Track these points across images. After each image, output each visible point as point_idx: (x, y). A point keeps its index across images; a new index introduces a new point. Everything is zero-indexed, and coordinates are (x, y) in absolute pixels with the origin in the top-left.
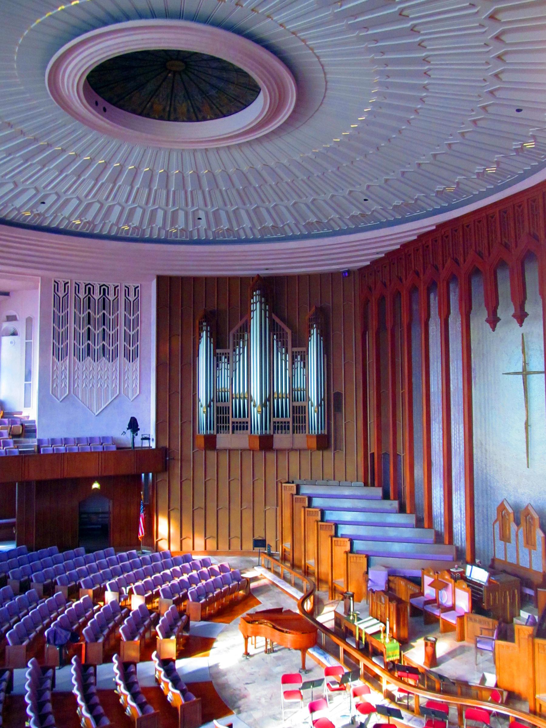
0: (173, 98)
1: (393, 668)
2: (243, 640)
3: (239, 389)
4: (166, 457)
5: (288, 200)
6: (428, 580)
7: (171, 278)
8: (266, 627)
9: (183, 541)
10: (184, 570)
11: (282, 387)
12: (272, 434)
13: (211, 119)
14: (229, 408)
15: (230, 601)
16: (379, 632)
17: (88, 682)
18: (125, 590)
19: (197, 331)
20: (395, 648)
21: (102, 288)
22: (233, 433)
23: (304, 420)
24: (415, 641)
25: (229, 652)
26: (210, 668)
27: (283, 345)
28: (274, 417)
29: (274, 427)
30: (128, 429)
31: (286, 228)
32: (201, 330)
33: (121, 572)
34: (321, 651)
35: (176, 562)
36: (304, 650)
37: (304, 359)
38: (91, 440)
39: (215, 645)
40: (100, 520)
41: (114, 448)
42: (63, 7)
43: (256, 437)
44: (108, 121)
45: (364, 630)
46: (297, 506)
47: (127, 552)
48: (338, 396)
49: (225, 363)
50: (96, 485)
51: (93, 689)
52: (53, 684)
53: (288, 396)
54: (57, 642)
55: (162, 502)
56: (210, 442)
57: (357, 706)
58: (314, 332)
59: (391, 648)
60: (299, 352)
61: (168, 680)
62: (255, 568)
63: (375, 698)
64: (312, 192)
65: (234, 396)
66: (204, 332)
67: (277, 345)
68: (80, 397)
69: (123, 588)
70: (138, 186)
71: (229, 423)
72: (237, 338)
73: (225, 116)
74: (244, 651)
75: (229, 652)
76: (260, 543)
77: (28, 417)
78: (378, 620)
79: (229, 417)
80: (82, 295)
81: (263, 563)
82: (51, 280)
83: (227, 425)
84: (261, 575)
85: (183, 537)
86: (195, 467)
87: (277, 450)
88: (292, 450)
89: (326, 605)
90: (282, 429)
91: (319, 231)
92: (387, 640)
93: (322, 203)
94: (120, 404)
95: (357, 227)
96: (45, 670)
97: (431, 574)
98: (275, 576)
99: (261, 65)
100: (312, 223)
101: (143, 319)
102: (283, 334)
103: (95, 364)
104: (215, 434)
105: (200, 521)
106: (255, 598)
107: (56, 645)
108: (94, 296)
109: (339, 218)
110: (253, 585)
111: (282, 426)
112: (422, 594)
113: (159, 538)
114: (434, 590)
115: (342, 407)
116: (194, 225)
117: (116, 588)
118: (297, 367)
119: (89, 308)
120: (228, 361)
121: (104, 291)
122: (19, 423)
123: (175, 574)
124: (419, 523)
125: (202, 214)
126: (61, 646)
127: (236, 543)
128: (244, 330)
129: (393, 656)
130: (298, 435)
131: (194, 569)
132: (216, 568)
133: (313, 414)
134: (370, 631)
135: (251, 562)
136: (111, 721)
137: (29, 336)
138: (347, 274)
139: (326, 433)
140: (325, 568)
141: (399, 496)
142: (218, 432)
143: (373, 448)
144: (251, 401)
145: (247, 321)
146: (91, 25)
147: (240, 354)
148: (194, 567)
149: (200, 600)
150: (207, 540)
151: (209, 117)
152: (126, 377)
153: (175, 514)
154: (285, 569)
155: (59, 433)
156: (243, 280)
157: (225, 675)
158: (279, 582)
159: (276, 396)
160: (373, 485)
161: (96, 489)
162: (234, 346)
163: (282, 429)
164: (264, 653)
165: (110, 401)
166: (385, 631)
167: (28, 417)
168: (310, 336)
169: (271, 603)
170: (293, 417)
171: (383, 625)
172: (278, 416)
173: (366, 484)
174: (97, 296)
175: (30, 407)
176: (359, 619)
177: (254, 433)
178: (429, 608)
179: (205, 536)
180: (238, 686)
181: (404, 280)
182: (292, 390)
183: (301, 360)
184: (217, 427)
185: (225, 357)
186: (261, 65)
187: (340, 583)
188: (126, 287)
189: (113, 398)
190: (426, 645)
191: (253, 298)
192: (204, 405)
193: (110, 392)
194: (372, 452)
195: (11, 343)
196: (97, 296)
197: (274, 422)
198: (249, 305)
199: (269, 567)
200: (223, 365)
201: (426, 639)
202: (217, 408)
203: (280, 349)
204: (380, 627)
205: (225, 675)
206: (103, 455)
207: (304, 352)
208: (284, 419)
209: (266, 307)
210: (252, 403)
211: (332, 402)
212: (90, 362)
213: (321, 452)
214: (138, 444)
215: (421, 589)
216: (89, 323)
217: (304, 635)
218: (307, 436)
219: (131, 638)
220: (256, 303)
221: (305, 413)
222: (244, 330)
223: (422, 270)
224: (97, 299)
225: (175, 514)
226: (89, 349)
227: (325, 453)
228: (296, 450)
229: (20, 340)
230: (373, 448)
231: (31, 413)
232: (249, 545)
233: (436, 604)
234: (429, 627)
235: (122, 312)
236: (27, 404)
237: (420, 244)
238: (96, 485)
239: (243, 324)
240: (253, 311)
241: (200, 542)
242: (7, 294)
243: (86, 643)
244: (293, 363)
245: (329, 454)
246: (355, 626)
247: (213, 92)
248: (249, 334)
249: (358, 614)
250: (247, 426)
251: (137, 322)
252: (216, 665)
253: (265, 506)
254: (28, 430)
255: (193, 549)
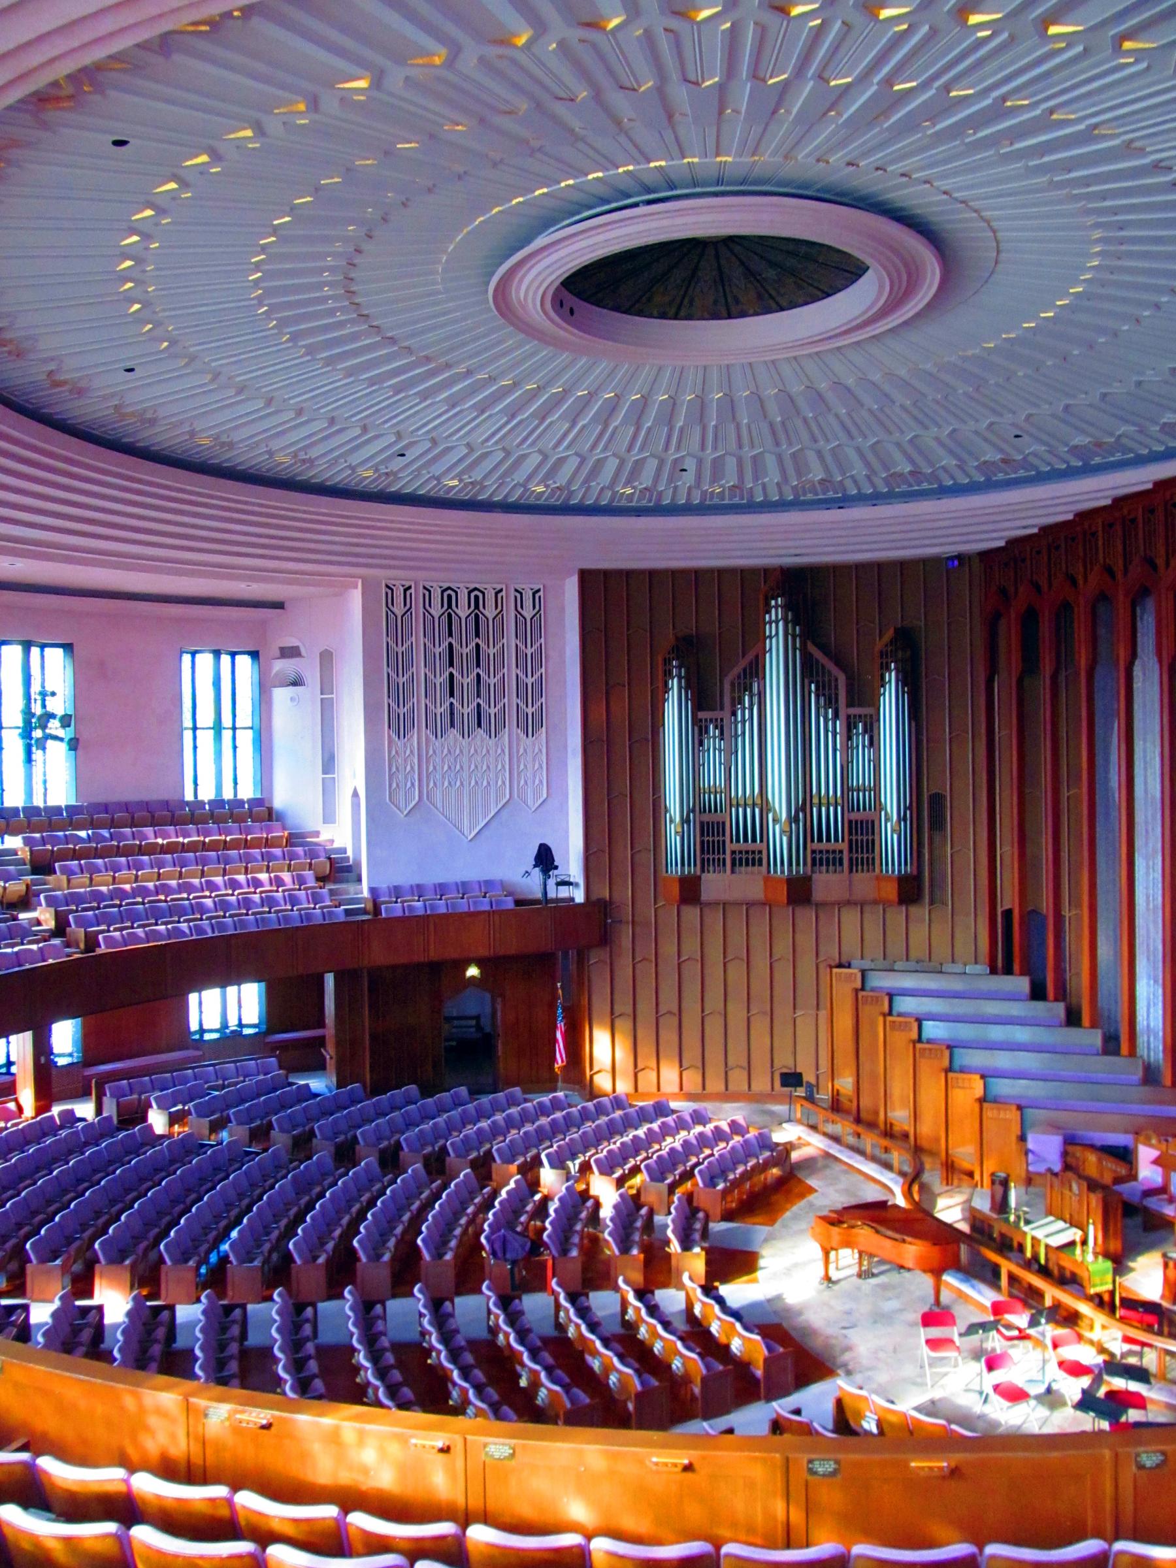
0: (693, 284)
1: (1105, 1303)
2: (819, 1254)
3: (745, 785)
4: (606, 918)
5: (865, 437)
6: (1146, 1154)
7: (606, 574)
8: (864, 1234)
9: (640, 1075)
10: (666, 1131)
11: (826, 778)
12: (809, 873)
13: (756, 314)
14: (724, 823)
15: (768, 1188)
16: (1072, 1244)
17: (374, 1331)
18: (574, 1166)
19: (660, 673)
20: (1105, 1272)
21: (472, 595)
22: (733, 872)
23: (870, 846)
24: (1134, 1260)
25: (793, 1271)
26: (769, 1301)
27: (830, 702)
28: (812, 840)
29: (814, 860)
30: (535, 866)
31: (849, 484)
32: (668, 674)
33: (461, 1125)
34: (960, 1275)
35: (643, 1116)
36: (937, 1272)
37: (872, 730)
38: (464, 888)
39: (762, 1262)
40: (454, 1030)
41: (509, 904)
42: (571, 182)
43: (779, 880)
44: (576, 331)
45: (1044, 1241)
46: (866, 1011)
47: (551, 1096)
48: (937, 801)
49: (714, 737)
50: (473, 971)
51: (385, 1342)
52: (244, 1335)
53: (839, 801)
54: (508, 1256)
55: (600, 1004)
56: (689, 891)
57: (1061, 1364)
58: (892, 677)
59: (1098, 1272)
60: (860, 716)
61: (509, 1330)
62: (784, 1125)
63: (1088, 1356)
64: (912, 423)
65: (734, 802)
66: (675, 680)
67: (817, 702)
68: (439, 805)
69: (570, 1164)
70: (585, 422)
71: (724, 853)
72: (739, 691)
73: (782, 309)
74: (822, 1273)
75: (793, 1271)
76: (792, 1079)
77: (332, 841)
78: (1065, 1221)
79: (724, 842)
80: (436, 610)
81: (799, 1115)
82: (379, 583)
83: (721, 857)
84: (800, 1138)
85: (640, 1066)
86: (660, 938)
87: (817, 905)
88: (849, 903)
89: (939, 1195)
90: (828, 865)
91: (911, 486)
92: (1090, 1257)
93: (934, 444)
94: (518, 818)
95: (988, 480)
96: (299, 1308)
97: (1154, 1141)
98: (830, 1142)
99: (892, 249)
100: (901, 475)
101: (551, 653)
102: (830, 681)
103: (465, 742)
104: (698, 873)
105: (669, 1036)
106: (800, 1181)
107: (506, 1260)
108: (458, 612)
109: (959, 466)
110: (795, 1156)
111: (828, 859)
112: (1132, 1176)
113: (596, 1069)
114: (1159, 1169)
115: (946, 823)
116: (671, 480)
117: (558, 1163)
118: (858, 746)
119: (450, 635)
120: (722, 733)
121: (476, 600)
122: (323, 854)
123: (652, 1137)
124: (1111, 1045)
125: (690, 464)
126: (514, 1263)
127: (738, 1080)
128: (751, 673)
129: (1102, 1284)
130: (860, 875)
131: (683, 1129)
132: (724, 1126)
133: (891, 835)
134: (1056, 1241)
135: (771, 1114)
136: (660, 1381)
137: (327, 686)
138: (956, 562)
139: (915, 873)
140: (928, 1128)
141: (1062, 993)
142: (703, 871)
143: (1008, 899)
144: (768, 810)
145: (757, 656)
146: (601, 199)
147: (743, 722)
148: (682, 1125)
149: (666, 1179)
150: (684, 1073)
151: (751, 311)
152: (522, 767)
153: (623, 1025)
154: (841, 1127)
155: (404, 875)
156: (745, 575)
157: (800, 1313)
158: (840, 1151)
159: (816, 800)
160: (1008, 971)
161: (473, 977)
162: (733, 705)
163: (828, 865)
164: (855, 1279)
165: (493, 813)
166: (1084, 1242)
167: (332, 841)
168: (883, 686)
169: (836, 1191)
170: (850, 841)
171: (1080, 1233)
172: (820, 839)
173: (993, 971)
174: (463, 611)
175: (334, 822)
176: (1027, 1222)
177: (775, 871)
178: (1152, 1203)
179: (681, 1066)
180: (831, 1331)
181: (1081, 582)
182: (847, 789)
183: (865, 731)
184: (703, 860)
185: (716, 727)
186: (892, 249)
187: (965, 1153)
188: (516, 590)
189: (500, 806)
190: (1166, 1266)
191: (769, 612)
192: (678, 819)
193: (493, 796)
194: (1007, 907)
195: (292, 699)
196: (463, 611)
197: (813, 852)
198: (761, 625)
199: (811, 1122)
200: (712, 742)
201: (1164, 1256)
202: (702, 824)
203: (822, 711)
204: (1075, 1234)
205: (800, 1313)
206: (497, 918)
207: (871, 716)
208: (832, 845)
209: (794, 630)
210: (770, 816)
211: (927, 811)
212: (456, 740)
213: (904, 908)
214: (552, 894)
215: (1131, 1169)
216: (451, 664)
217: (937, 1247)
218: (878, 878)
219: (625, 1249)
220: (777, 622)
221: (873, 833)
222: (751, 673)
223: (1121, 562)
224: (463, 615)
225: (623, 1025)
226: (452, 714)
227: (914, 910)
228: (856, 904)
229: (310, 692)
230: (1008, 899)
231: (341, 834)
232: (761, 1084)
233: (1165, 1196)
234: (1153, 1236)
235: (510, 640)
236: (329, 817)
237: (1117, 514)
238: (473, 971)
239: (751, 663)
240: (771, 637)
241: (670, 1075)
242: (279, 605)
243: (554, 1258)
244: (849, 738)
245: (920, 912)
246: (1025, 1233)
247: (771, 274)
248: (762, 683)
249: (1026, 1213)
250: (760, 860)
251: (538, 658)
252: (779, 1298)
253: (795, 1008)
254: (338, 870)
255: (659, 1089)
